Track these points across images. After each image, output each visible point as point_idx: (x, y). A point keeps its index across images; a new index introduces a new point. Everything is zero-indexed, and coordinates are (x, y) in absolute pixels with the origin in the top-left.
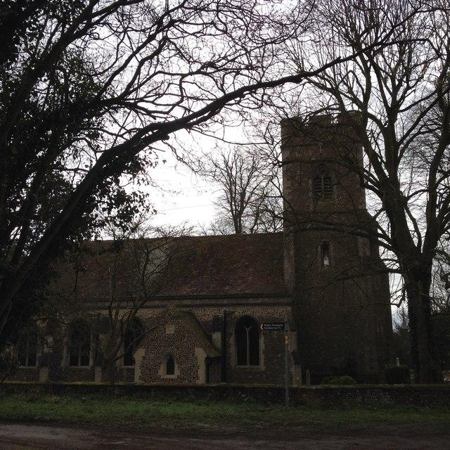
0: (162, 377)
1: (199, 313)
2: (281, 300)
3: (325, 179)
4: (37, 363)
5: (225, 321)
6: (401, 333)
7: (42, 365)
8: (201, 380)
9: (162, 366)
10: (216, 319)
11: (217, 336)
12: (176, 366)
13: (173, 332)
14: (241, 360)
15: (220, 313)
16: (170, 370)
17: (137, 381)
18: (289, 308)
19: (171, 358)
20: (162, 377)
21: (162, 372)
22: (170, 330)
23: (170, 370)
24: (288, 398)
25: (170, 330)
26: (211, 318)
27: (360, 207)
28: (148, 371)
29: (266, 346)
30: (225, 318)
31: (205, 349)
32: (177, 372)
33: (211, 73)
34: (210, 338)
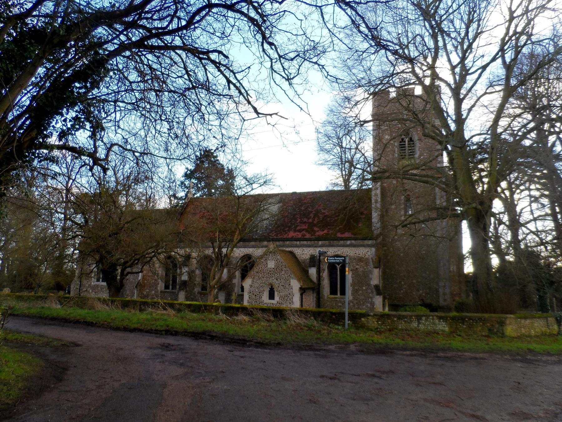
0: (265, 302)
1: (298, 251)
2: (366, 242)
3: (409, 142)
4: (178, 287)
5: (319, 259)
6: (225, 255)
7: (180, 289)
8: (296, 304)
9: (265, 293)
10: (312, 257)
11: (313, 272)
12: (276, 293)
13: (273, 267)
14: (333, 291)
15: (315, 251)
16: (272, 296)
17: (246, 303)
18: (373, 249)
19: (272, 287)
20: (265, 302)
21: (265, 298)
22: (271, 264)
23: (272, 296)
24: (347, 322)
25: (271, 264)
26: (308, 257)
27: (439, 165)
28: (254, 296)
29: (353, 280)
30: (320, 256)
31: (299, 280)
32: (277, 298)
33: (503, 57)
34: (306, 272)
